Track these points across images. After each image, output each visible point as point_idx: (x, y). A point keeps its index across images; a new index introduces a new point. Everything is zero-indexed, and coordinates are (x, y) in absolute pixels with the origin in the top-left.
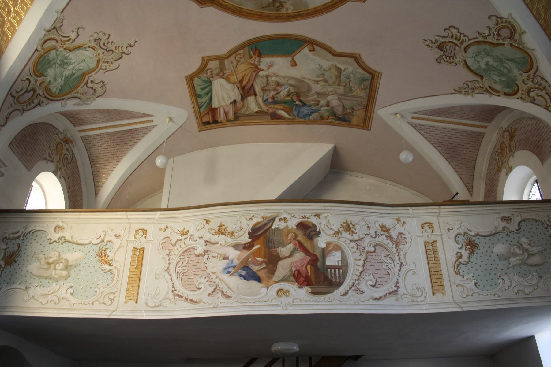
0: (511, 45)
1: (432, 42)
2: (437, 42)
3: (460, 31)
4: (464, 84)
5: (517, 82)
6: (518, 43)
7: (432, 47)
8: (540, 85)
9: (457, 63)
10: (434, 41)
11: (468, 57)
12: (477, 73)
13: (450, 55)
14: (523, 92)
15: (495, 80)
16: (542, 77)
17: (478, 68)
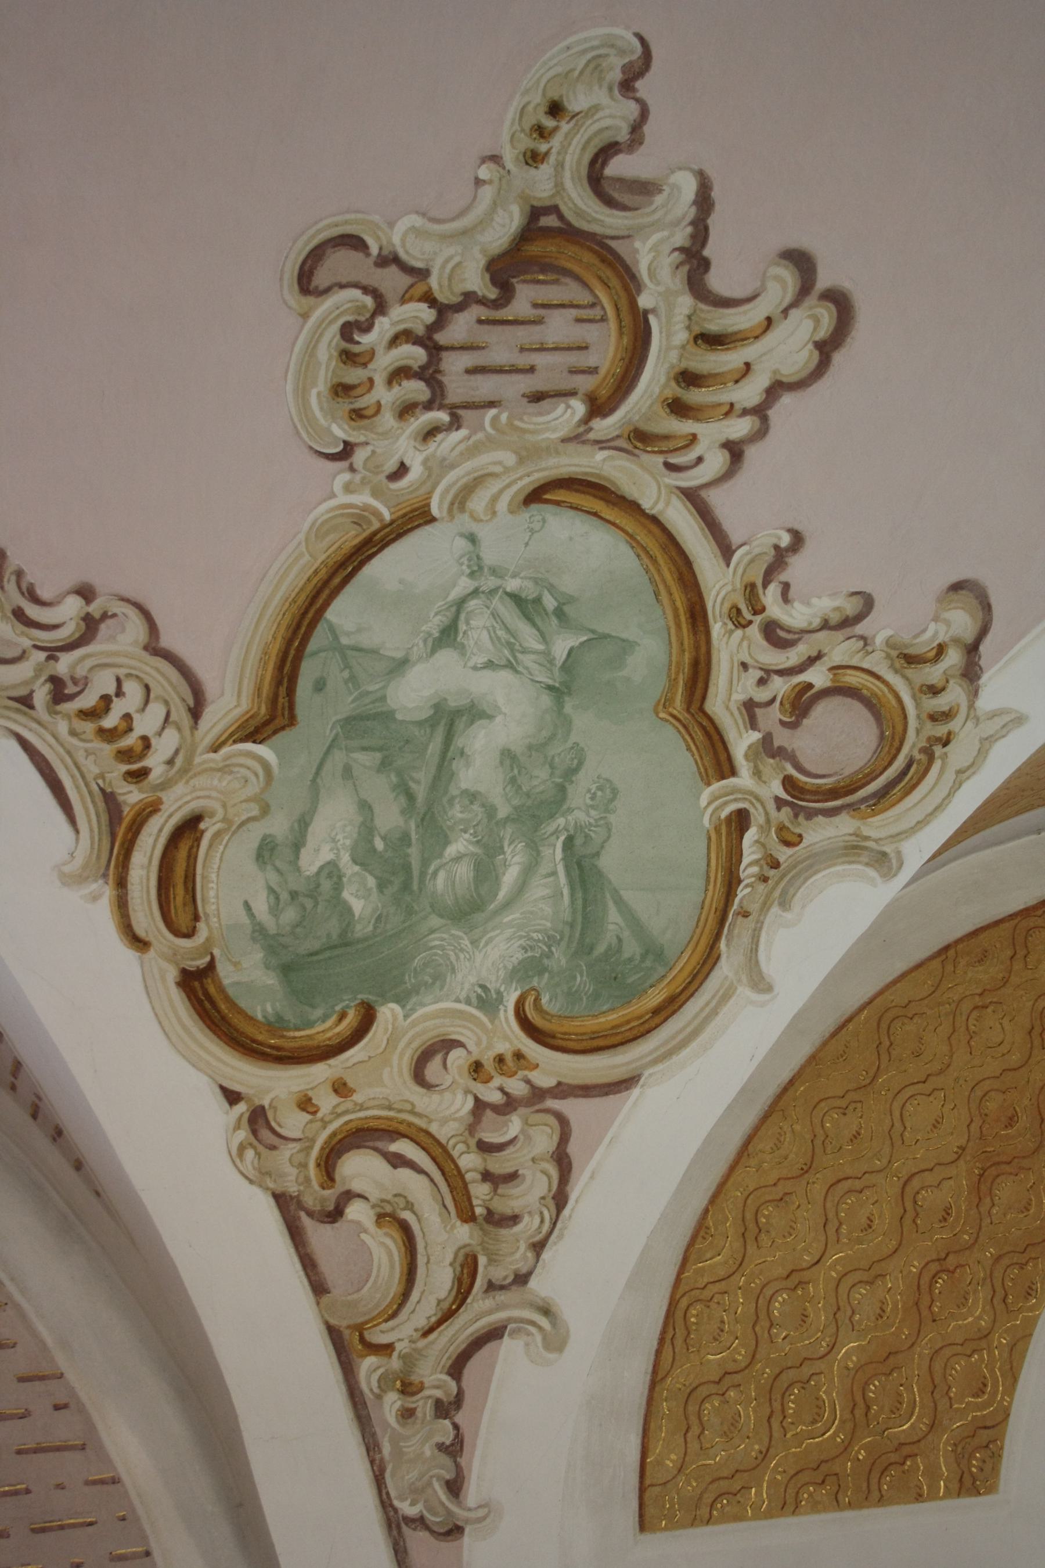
0: (740, 821)
1: (607, 151)
2: (609, 202)
3: (787, 400)
4: (86, 593)
5: (388, 1013)
6: (775, 865)
7: (534, 158)
8: (487, 1176)
9: (360, 456)
10: (617, 167)
11: (472, 539)
12: (308, 672)
13: (454, 365)
14: (327, 1102)
15: (297, 846)
16: (573, 1149)
17: (374, 652)
